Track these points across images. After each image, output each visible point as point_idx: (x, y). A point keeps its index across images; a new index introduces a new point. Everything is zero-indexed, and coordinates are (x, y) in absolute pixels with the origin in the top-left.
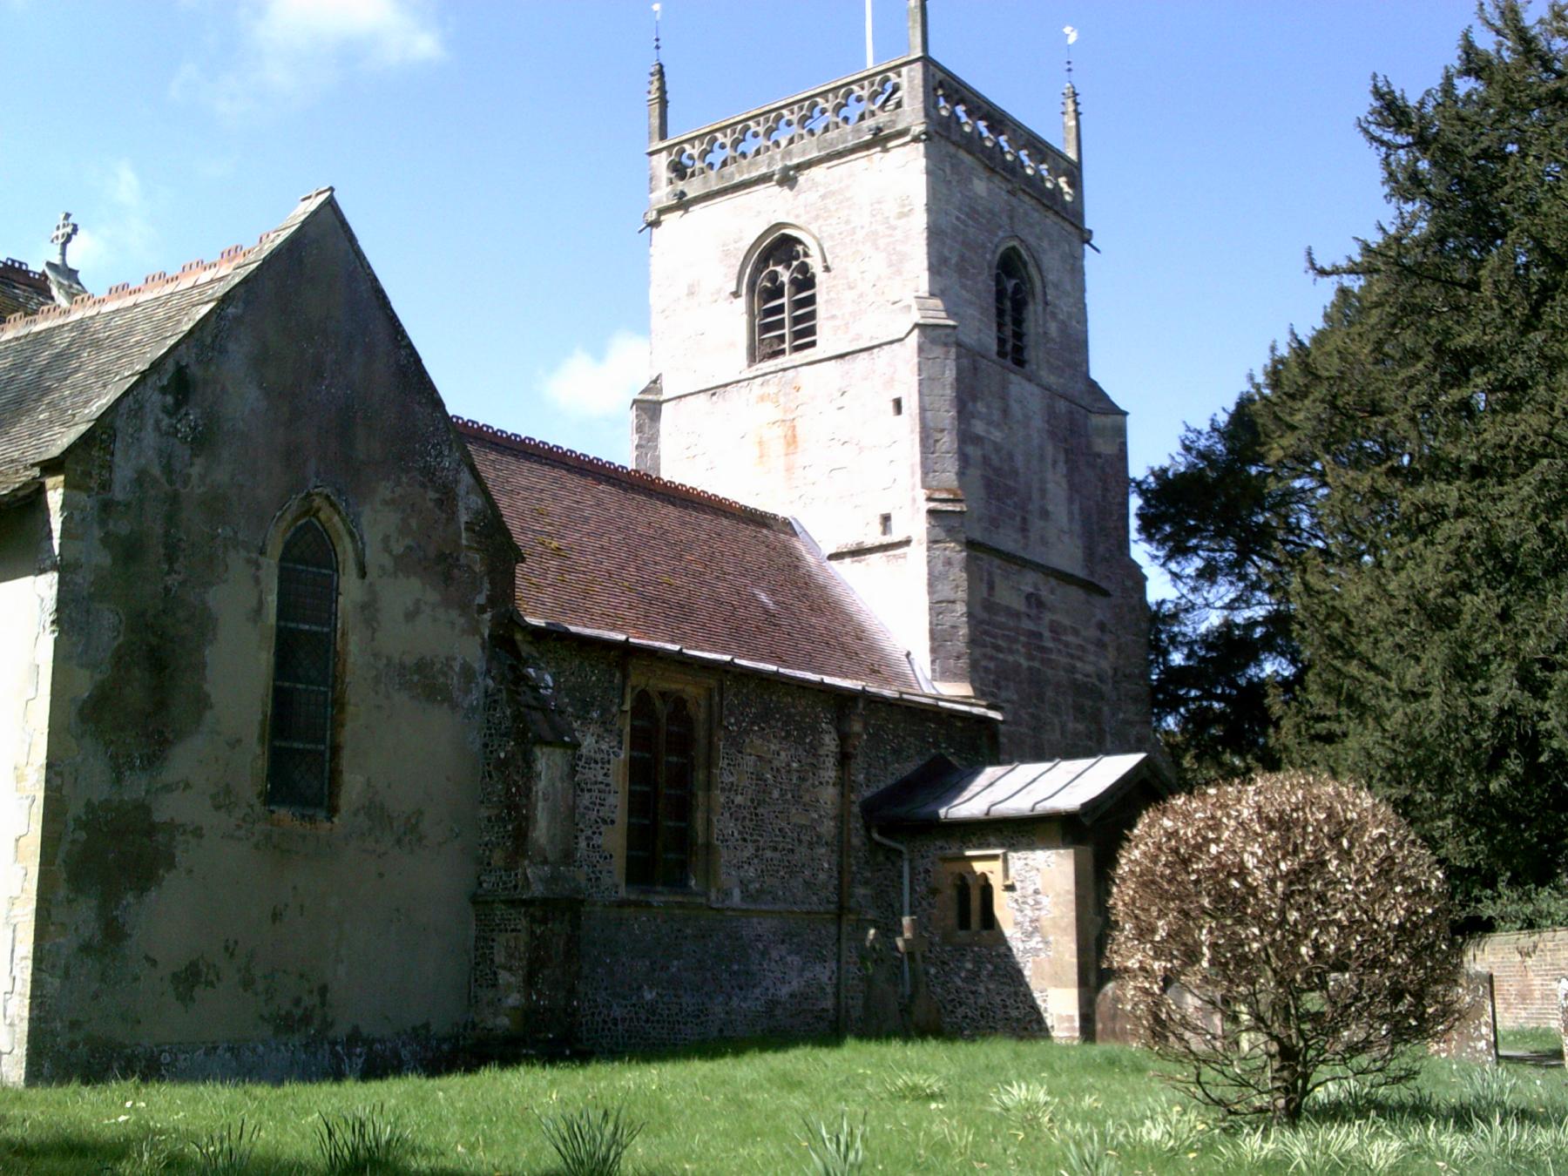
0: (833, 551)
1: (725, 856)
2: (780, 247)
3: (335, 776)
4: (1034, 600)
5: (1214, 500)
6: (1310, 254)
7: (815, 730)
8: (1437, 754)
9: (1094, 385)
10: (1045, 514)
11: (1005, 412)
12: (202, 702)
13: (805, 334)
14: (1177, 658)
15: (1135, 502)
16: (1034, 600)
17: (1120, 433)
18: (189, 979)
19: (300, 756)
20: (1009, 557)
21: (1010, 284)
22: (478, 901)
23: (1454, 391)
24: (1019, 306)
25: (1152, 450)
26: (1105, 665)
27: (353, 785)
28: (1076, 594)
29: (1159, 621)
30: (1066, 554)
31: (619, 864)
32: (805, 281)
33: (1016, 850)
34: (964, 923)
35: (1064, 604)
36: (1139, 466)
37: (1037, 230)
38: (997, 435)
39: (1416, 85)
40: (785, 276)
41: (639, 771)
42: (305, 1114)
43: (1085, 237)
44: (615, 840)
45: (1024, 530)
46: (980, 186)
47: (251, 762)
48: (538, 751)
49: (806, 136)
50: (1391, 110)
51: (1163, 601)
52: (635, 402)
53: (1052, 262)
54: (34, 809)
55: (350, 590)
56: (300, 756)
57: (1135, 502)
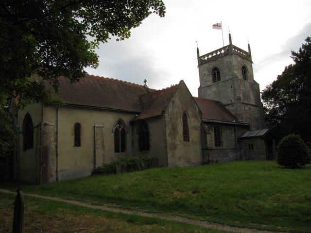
0: (199, 50)
1: (224, 143)
2: (215, 69)
3: (189, 138)
4: (250, 109)
5: (268, 94)
6: (145, 81)
7: (264, 128)
8: (97, 31)
9: (254, 81)
10: (250, 98)
11: (245, 86)
12: (178, 132)
13: (219, 79)
14: (268, 113)
15: (261, 94)
16: (250, 109)
17: (259, 87)
18: (180, 158)
19: (186, 136)
20: (246, 104)
21: (244, 70)
22: (202, 149)
23: (124, 213)
24: (245, 72)
25: (262, 88)
26: (259, 115)
27: (190, 139)
28: (255, 107)
29: (265, 108)
30: (253, 102)
31: (214, 145)
32: (219, 72)
33: (265, 142)
34: (250, 148)
35: (253, 108)
36: (261, 91)
37: (246, 63)
38: (244, 89)
39: (297, 51)
40: (216, 72)
41: (215, 135)
42: (233, 230)
43: (252, 62)
44: (213, 142)
45: (248, 100)
46: (239, 59)
47: (182, 138)
48: (208, 135)
49: (94, 42)
50: (294, 54)
51: (301, 49)
52: (160, 15)
53: (249, 67)
54: (54, 168)
55: (188, 120)
56: (186, 136)
57: (261, 94)
